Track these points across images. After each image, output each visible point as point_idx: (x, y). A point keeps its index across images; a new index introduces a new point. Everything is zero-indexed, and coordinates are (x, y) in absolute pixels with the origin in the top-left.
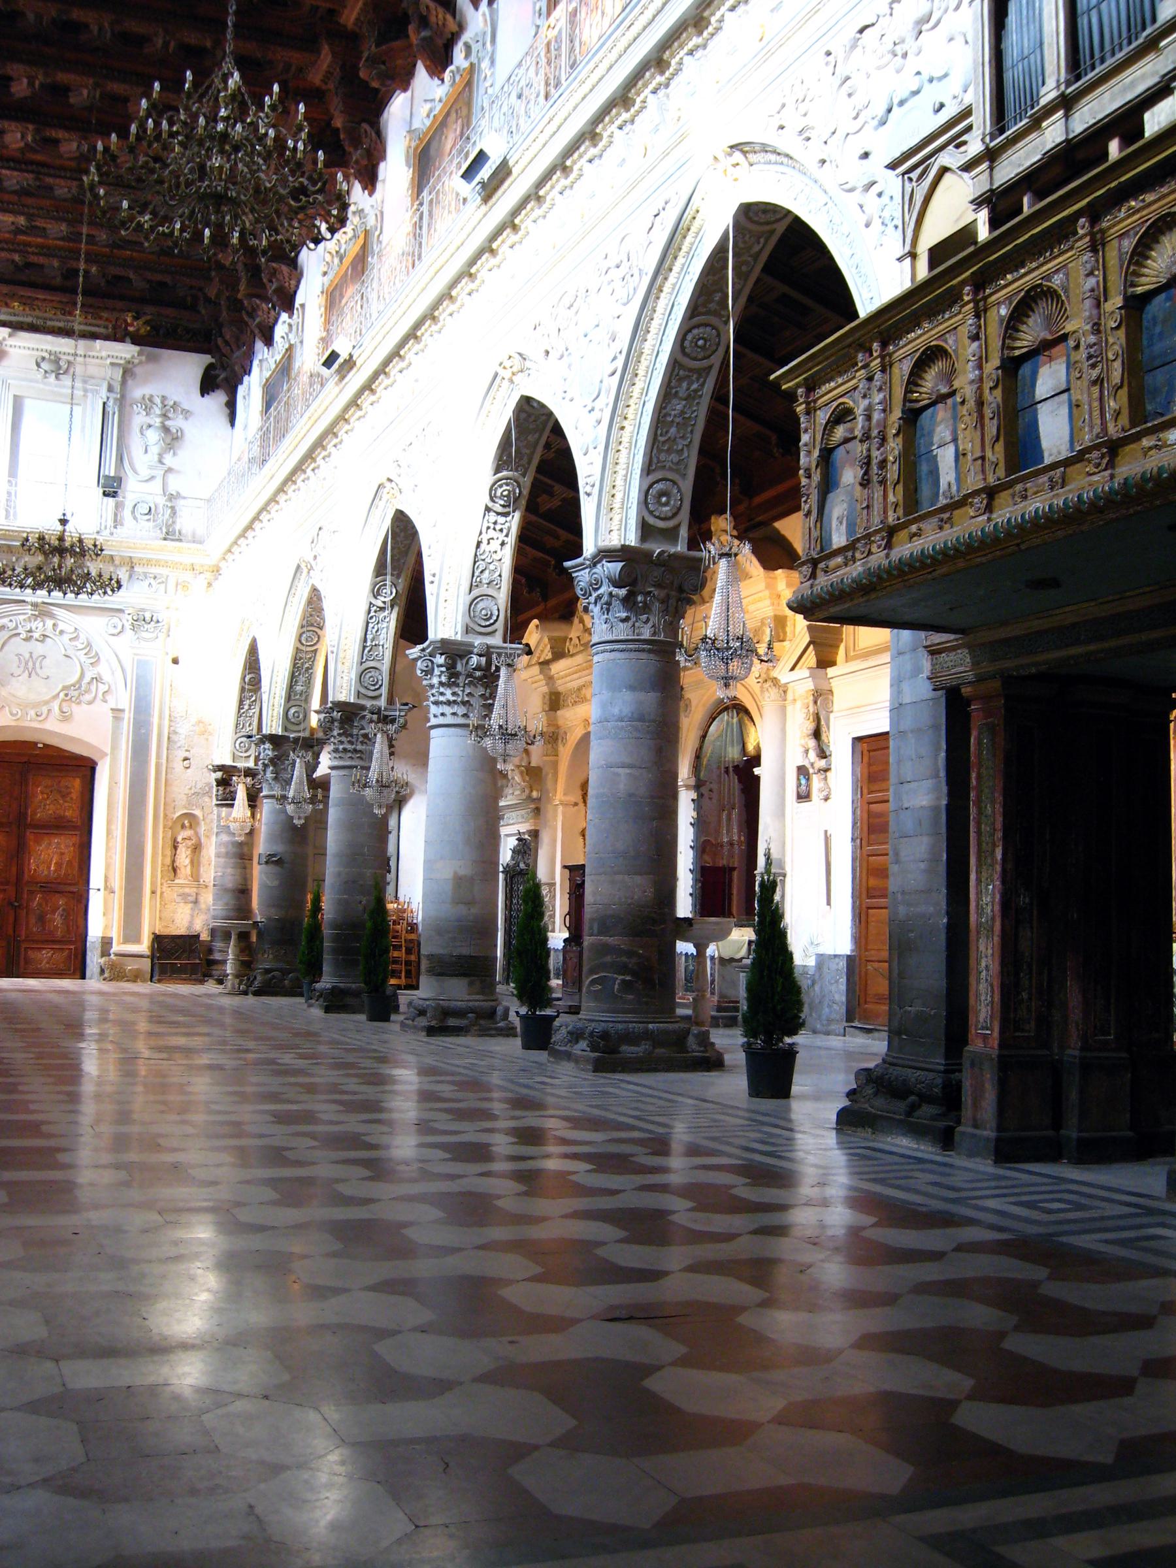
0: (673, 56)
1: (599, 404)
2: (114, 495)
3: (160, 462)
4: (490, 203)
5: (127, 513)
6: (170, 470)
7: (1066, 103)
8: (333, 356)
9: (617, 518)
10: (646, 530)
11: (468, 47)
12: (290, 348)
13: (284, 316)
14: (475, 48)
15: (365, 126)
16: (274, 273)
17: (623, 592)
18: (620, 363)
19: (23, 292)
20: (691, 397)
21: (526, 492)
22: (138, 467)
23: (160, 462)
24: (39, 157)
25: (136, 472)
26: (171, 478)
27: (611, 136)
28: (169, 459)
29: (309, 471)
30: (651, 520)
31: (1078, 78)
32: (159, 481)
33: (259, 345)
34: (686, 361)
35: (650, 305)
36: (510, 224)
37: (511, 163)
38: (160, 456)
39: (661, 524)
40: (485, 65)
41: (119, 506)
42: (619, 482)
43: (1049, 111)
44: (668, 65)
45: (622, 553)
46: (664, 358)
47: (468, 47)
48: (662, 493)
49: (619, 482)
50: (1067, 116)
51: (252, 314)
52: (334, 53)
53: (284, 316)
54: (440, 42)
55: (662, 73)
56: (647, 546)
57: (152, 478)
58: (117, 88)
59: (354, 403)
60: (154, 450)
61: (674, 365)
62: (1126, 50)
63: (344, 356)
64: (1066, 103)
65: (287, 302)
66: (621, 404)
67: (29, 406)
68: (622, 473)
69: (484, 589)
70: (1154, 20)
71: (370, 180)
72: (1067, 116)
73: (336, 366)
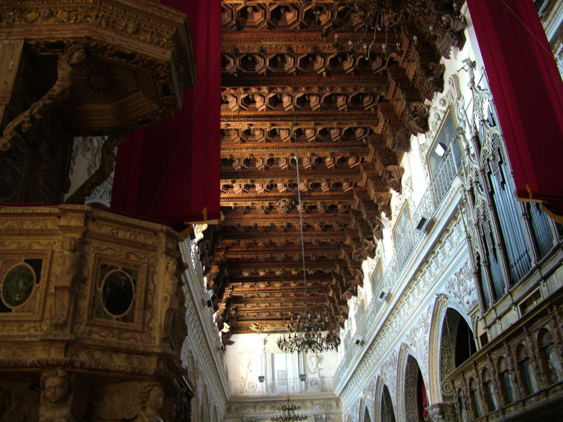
0: (450, 227)
1: (426, 361)
2: (304, 380)
3: (317, 367)
4: (429, 235)
5: (309, 385)
6: (320, 369)
7: (539, 267)
8: (383, 294)
9: (436, 394)
10: (444, 397)
11: (378, 251)
12: (349, 331)
13: (346, 320)
14: (380, 252)
15: (357, 269)
16: (341, 309)
17: (441, 416)
18: (428, 350)
19: (270, 322)
20: (449, 357)
21: (417, 380)
22: (311, 370)
23: (317, 367)
24: (269, 288)
25: (310, 371)
26: (321, 371)
27: (453, 229)
28: (319, 366)
29: (379, 340)
30: (445, 394)
31: (541, 258)
32: (317, 373)
33: (341, 328)
34: (445, 348)
35: (432, 334)
36: (438, 241)
37: (392, 292)
38: (317, 365)
39: (449, 395)
40: (383, 258)
41: (306, 384)
42: (435, 384)
43: (534, 269)
44: (457, 217)
45: (439, 405)
46: (439, 348)
47: (378, 251)
48: (446, 386)
49: (435, 384)
50: (540, 271)
51: (337, 319)
52: (345, 250)
53: (346, 320)
54: (372, 250)
55: (456, 220)
56: (446, 402)
57: (315, 372)
58: (287, 269)
59: (367, 352)
60: (315, 363)
61: (442, 350)
62: (527, 274)
63: (386, 292)
64: (539, 267)
65: (346, 316)
66: (431, 362)
67: (275, 355)
68: (435, 381)
69: (411, 411)
70: (531, 267)
71: (362, 284)
72: (540, 271)
73: (424, 227)
